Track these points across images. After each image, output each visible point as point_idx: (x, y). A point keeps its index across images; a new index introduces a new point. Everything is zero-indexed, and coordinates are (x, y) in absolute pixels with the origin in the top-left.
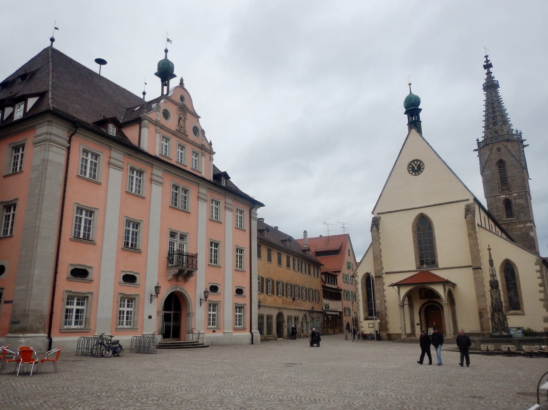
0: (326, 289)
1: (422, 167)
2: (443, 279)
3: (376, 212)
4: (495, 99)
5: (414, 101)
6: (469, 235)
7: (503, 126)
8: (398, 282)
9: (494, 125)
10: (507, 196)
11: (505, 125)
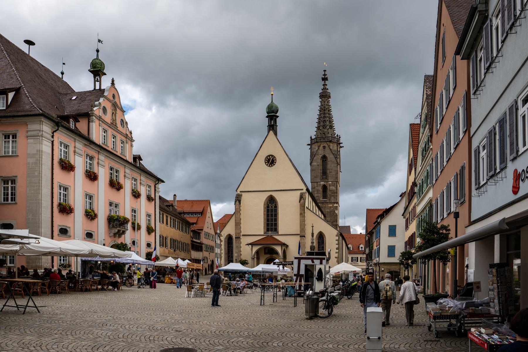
0: (193, 243)
1: (275, 161)
2: (281, 242)
6: (301, 214)
8: (252, 243)
9: (324, 127)
10: (325, 183)
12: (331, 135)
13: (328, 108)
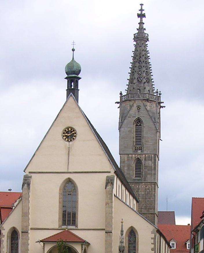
2: (82, 239)
3: (29, 170)
4: (144, 53)
5: (75, 70)
6: (107, 204)
7: (146, 84)
8: (45, 239)
11: (148, 83)
12: (149, 91)
13: (146, 54)
